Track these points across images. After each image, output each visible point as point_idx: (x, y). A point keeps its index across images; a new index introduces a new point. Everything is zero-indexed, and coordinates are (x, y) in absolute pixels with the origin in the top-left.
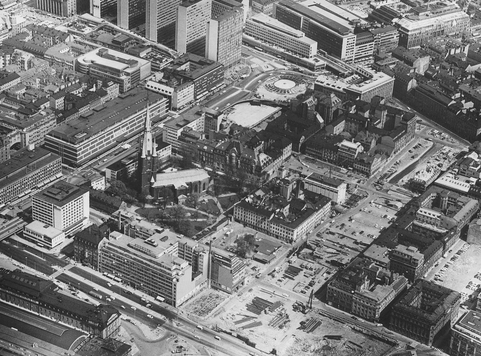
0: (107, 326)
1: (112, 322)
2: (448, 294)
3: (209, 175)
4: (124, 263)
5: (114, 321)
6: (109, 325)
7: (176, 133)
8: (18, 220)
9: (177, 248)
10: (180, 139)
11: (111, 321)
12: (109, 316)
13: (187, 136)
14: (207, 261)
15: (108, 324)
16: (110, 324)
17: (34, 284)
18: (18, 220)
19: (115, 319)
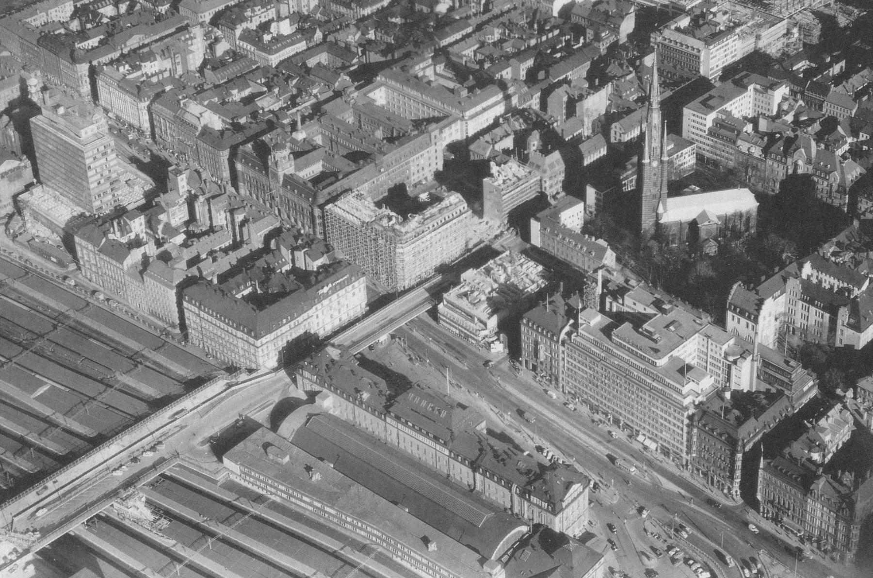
0: (562, 510)
1: (572, 501)
2: (255, 430)
3: (758, 200)
4: (625, 377)
5: (575, 499)
6: (567, 507)
7: (704, 122)
8: (444, 321)
9: (695, 354)
10: (712, 133)
11: (570, 500)
12: (568, 486)
13: (722, 126)
14: (748, 377)
15: (564, 505)
16: (569, 504)
17: (443, 414)
18: (444, 321)
19: (579, 495)
